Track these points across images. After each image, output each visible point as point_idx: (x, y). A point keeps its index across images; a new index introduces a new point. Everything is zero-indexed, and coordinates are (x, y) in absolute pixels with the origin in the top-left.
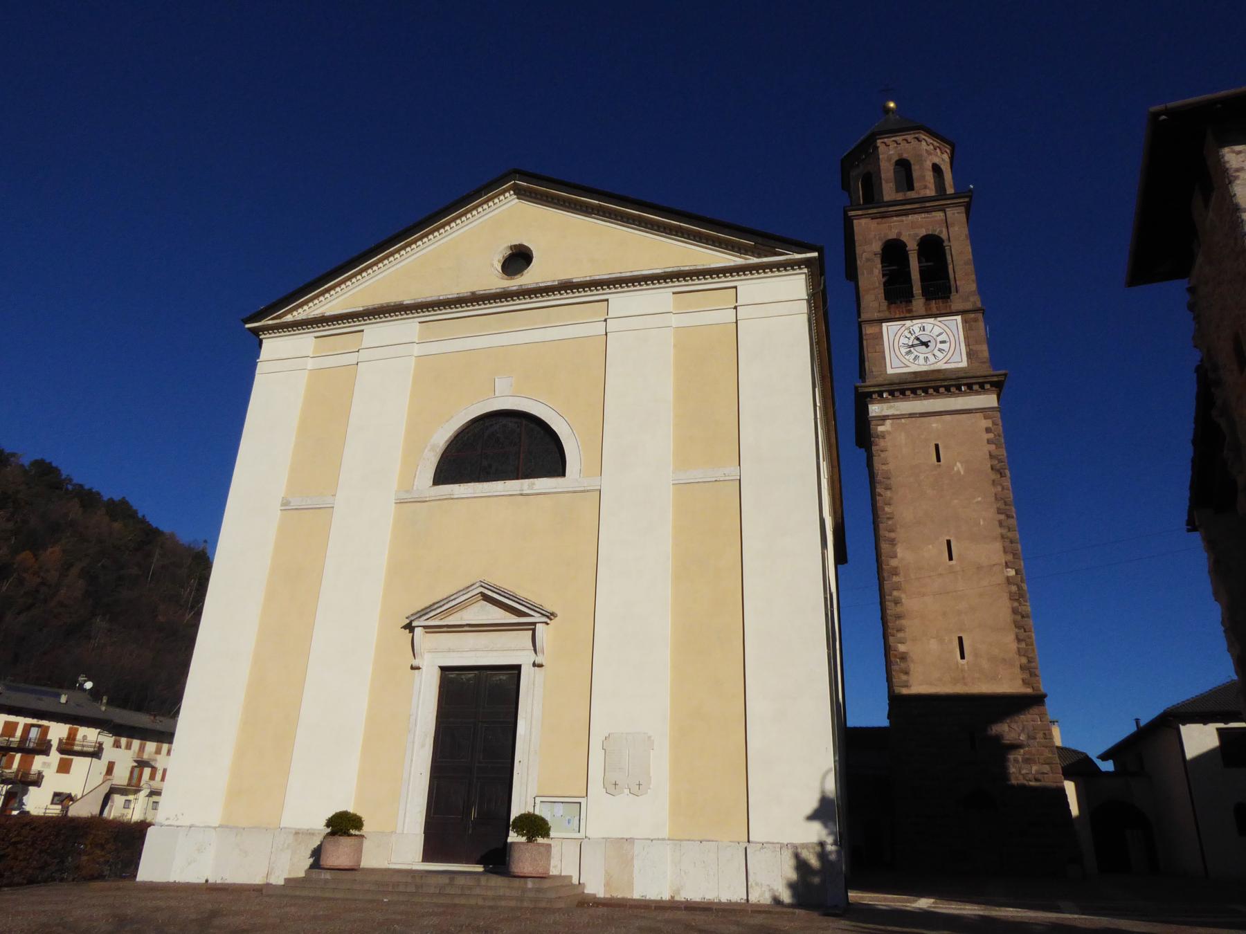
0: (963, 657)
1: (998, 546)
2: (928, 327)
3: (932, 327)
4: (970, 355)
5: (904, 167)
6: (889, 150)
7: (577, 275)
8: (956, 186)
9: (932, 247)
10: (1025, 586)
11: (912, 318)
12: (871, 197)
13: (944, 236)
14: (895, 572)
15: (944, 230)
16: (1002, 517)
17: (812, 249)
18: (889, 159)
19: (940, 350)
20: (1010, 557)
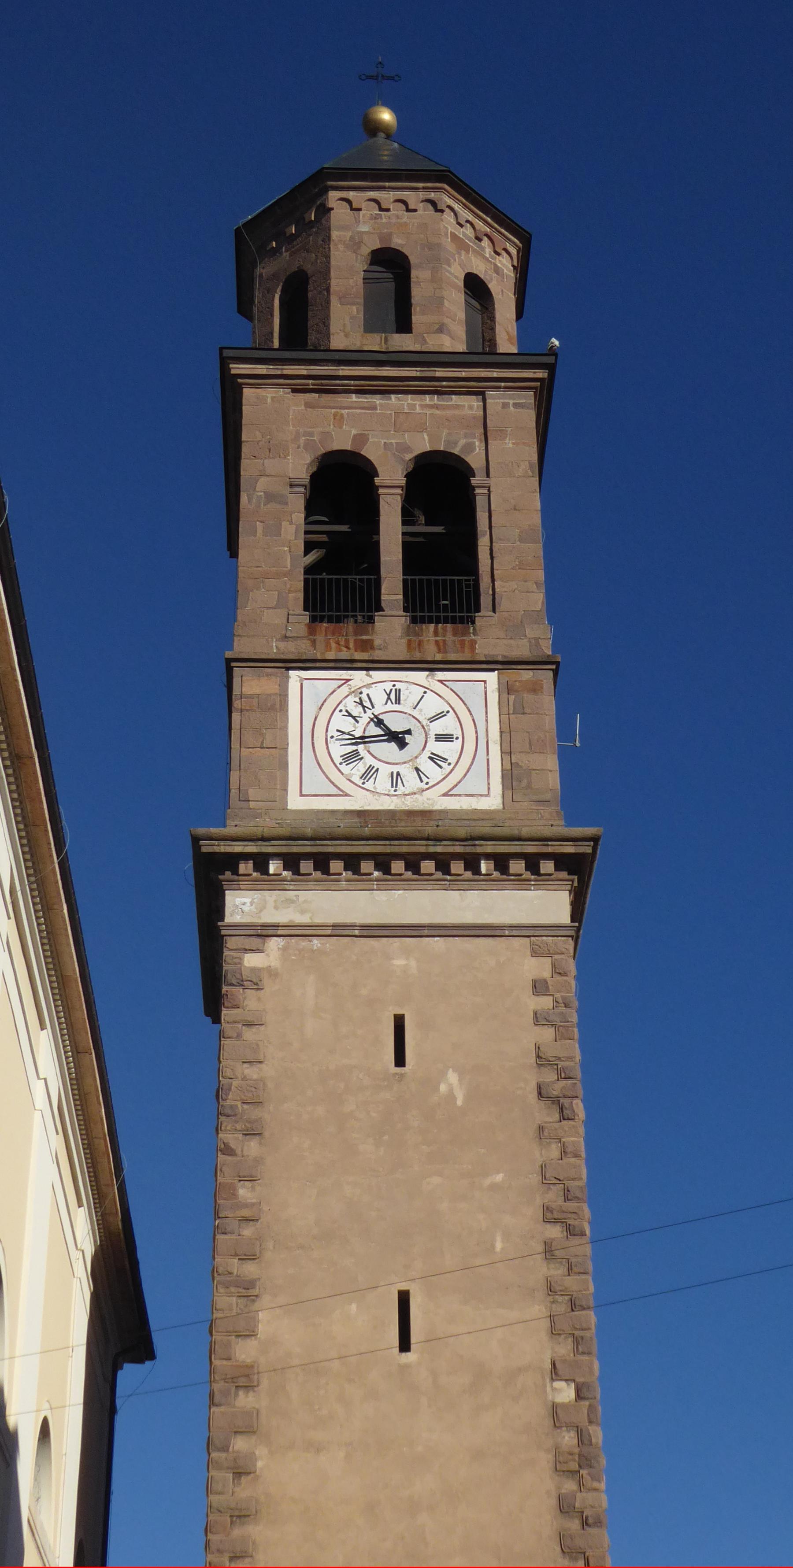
1: (538, 1310)
2: (410, 694)
3: (420, 696)
5: (391, 267)
6: (357, 224)
8: (522, 337)
9: (442, 484)
10: (597, 1434)
11: (371, 665)
12: (301, 333)
13: (475, 460)
14: (245, 1379)
15: (479, 446)
16: (555, 1232)
18: (355, 244)
19: (434, 758)
20: (564, 1349)
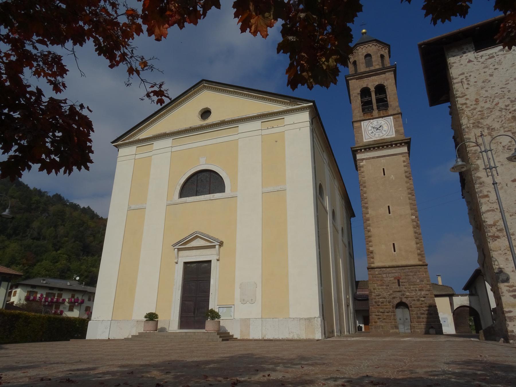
0: (395, 251)
1: (408, 207)
4: (396, 131)
7: (227, 118)
9: (381, 89)
11: (373, 119)
17: (310, 102)
18: (363, 54)
